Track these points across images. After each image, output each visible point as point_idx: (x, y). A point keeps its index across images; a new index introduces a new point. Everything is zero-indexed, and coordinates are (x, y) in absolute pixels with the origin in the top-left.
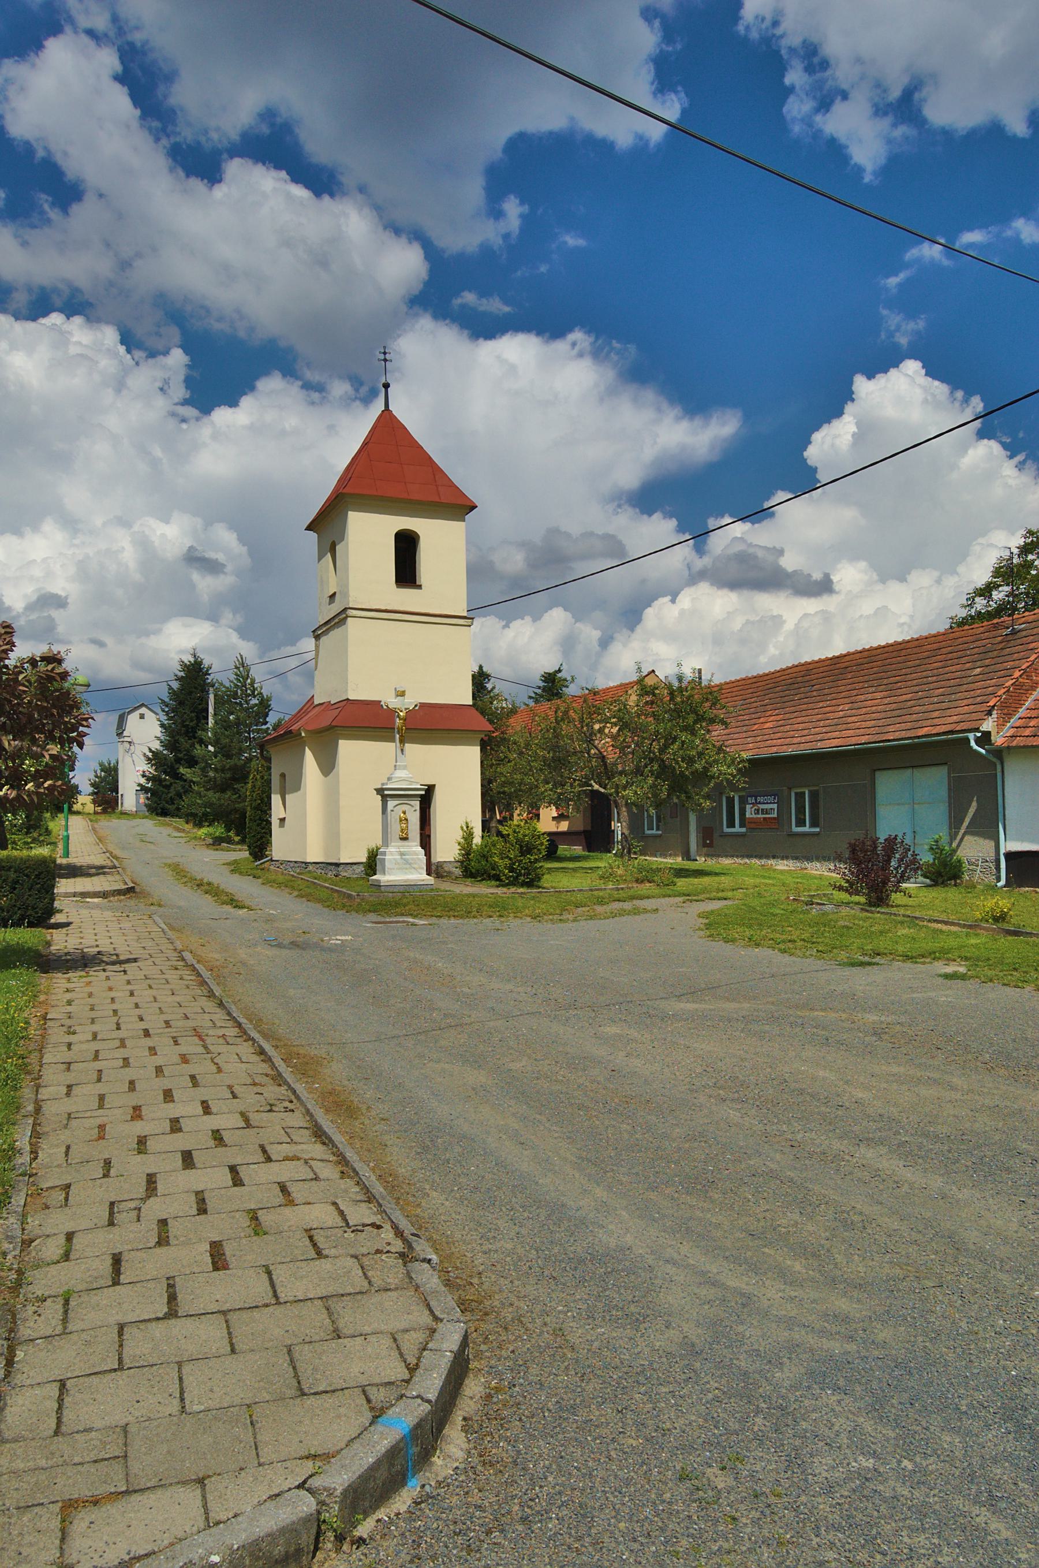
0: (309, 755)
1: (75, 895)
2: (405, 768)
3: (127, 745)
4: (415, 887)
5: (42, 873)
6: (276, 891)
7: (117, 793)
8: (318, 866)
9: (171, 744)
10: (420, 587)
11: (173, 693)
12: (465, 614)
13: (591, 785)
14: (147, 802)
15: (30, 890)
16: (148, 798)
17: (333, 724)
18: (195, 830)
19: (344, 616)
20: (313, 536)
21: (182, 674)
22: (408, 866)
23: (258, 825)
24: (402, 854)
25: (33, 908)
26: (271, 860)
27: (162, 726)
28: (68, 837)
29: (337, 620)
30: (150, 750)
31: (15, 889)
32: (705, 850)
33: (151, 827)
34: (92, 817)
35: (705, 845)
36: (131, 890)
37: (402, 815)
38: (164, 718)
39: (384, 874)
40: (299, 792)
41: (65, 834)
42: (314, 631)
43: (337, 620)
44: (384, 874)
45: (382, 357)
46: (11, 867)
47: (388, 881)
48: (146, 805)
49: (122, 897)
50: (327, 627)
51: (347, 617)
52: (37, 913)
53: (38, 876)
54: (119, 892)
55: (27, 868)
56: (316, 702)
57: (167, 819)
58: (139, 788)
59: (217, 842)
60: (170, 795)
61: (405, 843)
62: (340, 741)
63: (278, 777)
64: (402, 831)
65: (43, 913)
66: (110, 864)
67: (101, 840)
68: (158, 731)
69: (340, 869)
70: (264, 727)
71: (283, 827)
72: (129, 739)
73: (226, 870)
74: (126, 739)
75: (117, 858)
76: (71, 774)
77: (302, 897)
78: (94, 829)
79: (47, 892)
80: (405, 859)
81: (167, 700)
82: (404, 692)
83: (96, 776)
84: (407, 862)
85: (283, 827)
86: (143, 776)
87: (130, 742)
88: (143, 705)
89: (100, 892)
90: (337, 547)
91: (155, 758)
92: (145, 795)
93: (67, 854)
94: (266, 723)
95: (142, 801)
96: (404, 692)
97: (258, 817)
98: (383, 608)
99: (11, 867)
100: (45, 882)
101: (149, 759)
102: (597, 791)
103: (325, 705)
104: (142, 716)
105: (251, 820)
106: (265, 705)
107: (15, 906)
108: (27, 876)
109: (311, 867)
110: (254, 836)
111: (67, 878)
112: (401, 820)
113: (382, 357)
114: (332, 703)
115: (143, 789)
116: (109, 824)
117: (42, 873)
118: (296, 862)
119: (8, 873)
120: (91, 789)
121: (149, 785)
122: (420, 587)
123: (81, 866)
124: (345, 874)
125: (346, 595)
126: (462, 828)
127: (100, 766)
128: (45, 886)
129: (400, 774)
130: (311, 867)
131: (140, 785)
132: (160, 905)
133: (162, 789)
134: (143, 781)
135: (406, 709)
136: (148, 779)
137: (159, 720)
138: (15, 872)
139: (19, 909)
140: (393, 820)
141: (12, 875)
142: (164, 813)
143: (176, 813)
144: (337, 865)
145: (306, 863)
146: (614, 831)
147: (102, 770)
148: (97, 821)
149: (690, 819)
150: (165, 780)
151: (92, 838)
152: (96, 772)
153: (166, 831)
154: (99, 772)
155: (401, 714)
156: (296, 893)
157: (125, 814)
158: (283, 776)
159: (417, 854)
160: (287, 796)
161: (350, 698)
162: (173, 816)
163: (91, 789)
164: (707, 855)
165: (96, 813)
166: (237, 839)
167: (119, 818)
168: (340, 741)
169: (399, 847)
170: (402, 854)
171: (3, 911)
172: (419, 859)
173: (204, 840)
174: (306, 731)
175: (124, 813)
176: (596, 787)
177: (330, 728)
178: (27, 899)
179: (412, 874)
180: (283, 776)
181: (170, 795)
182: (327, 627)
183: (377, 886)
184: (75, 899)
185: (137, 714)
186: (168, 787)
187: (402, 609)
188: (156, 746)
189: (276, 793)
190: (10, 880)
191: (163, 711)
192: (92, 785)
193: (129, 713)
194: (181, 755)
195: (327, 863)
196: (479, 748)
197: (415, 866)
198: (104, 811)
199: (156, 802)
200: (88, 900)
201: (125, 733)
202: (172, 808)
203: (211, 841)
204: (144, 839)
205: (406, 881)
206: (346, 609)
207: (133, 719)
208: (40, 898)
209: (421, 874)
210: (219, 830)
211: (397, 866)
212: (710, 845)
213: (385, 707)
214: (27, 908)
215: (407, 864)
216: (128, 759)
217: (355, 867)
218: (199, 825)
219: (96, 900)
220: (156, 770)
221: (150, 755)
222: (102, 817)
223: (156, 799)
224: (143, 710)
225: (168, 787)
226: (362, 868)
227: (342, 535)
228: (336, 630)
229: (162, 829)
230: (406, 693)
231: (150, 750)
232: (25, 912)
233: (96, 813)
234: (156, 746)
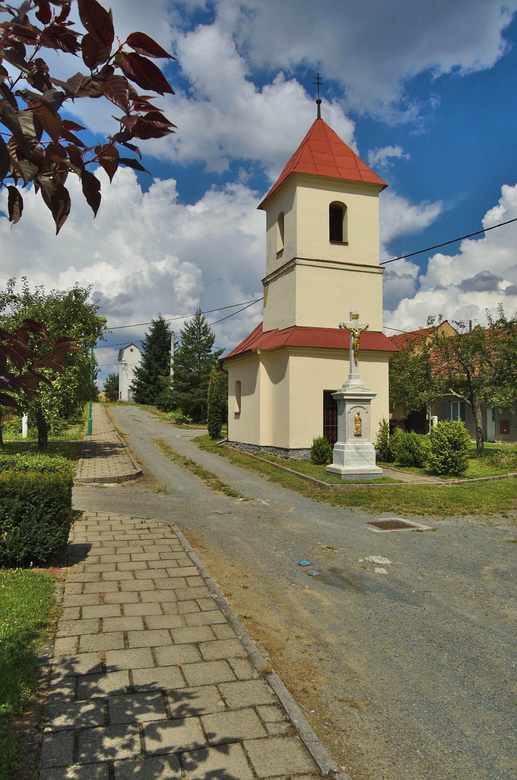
0: (262, 368)
1: (94, 480)
2: (358, 377)
3: (124, 365)
4: (368, 476)
5: (54, 500)
6: (247, 471)
7: (118, 391)
8: (268, 449)
9: (148, 364)
10: (346, 244)
11: (149, 338)
12: (378, 265)
13: (450, 392)
14: (134, 396)
15: (38, 521)
16: (134, 394)
17: (286, 344)
18: (163, 413)
19: (293, 264)
20: (263, 213)
21: (153, 327)
22: (362, 458)
23: (216, 416)
24: (357, 448)
25: (42, 544)
26: (227, 441)
27: (143, 355)
28: (91, 421)
29: (285, 269)
30: (136, 368)
31: (20, 520)
32: (502, 436)
33: (137, 410)
34: (106, 404)
35: (502, 432)
36: (140, 474)
37: (357, 416)
38: (143, 351)
39: (343, 465)
40: (253, 395)
41: (90, 419)
42: (263, 280)
43: (285, 269)
44: (343, 465)
45: (316, 81)
46: (15, 494)
47: (347, 471)
48: (133, 398)
49: (133, 481)
50: (276, 275)
51: (296, 264)
52: (46, 549)
53: (48, 505)
54: (130, 477)
55: (35, 494)
56: (264, 330)
57: (146, 406)
58: (130, 389)
59: (179, 422)
60: (146, 393)
61: (358, 439)
62: (290, 357)
63: (234, 384)
64: (357, 429)
65: (54, 550)
66: (119, 442)
67: (111, 420)
68: (140, 358)
69: (290, 453)
70: (209, 354)
71: (239, 418)
72: (125, 362)
73: (195, 446)
74: (123, 362)
75: (121, 435)
76: (95, 381)
77: (276, 481)
78: (106, 412)
79: (60, 523)
80: (359, 453)
81: (145, 342)
82: (358, 315)
83: (107, 382)
84: (361, 455)
85: (239, 418)
86: (133, 382)
87: (125, 364)
88: (132, 344)
89: (115, 478)
90: (285, 216)
91: (139, 373)
92: (133, 393)
93: (90, 433)
94: (210, 351)
95: (131, 395)
96: (358, 315)
97: (215, 411)
98: (321, 259)
99: (15, 494)
100: (57, 512)
101: (135, 373)
102: (455, 396)
103: (272, 333)
104: (132, 350)
105: (210, 412)
106: (211, 341)
107: (20, 541)
108: (35, 504)
109: (262, 450)
110: (212, 423)
111: (89, 458)
112: (356, 420)
113: (316, 81)
114: (280, 330)
115: (133, 389)
116: (114, 408)
117: (54, 500)
118: (250, 445)
119: (12, 500)
120: (105, 389)
121: (136, 387)
122: (346, 244)
123: (100, 444)
124: (293, 457)
125: (294, 248)
126: (380, 423)
127: (110, 376)
128: (58, 516)
129: (354, 382)
130: (262, 450)
131: (130, 387)
132: (166, 493)
133: (142, 389)
134: (132, 384)
135: (359, 329)
136: (135, 384)
137: (141, 352)
138: (20, 499)
139: (25, 544)
140: (349, 420)
141: (17, 504)
142: (143, 402)
143: (151, 402)
144: (287, 450)
145: (259, 447)
146: (428, 421)
147: (110, 379)
148: (107, 407)
149: (488, 415)
150: (144, 384)
151: (105, 419)
152: (107, 379)
153: (147, 413)
154: (109, 380)
155: (356, 333)
156: (268, 477)
157: (123, 402)
158: (239, 383)
159: (368, 449)
160: (242, 397)
161: (297, 325)
162: (148, 404)
163: (105, 389)
164: (504, 440)
165: (107, 402)
166: (190, 420)
167: (119, 405)
168: (290, 357)
169: (354, 442)
170: (357, 448)
171: (5, 548)
172: (370, 452)
173: (170, 420)
174: (261, 350)
175: (122, 402)
176: (454, 394)
177: (284, 347)
178: (36, 532)
179: (365, 464)
180: (239, 383)
181: (146, 393)
182: (276, 275)
183: (338, 474)
184: (95, 484)
185: (129, 349)
186: (146, 388)
187: (334, 260)
188: (139, 366)
189: (232, 395)
190: (15, 508)
191: (143, 347)
192: (105, 387)
193: (125, 348)
194: (153, 371)
195: (277, 448)
196: (388, 364)
197: (367, 458)
198: (111, 400)
199: (139, 396)
200: (106, 485)
201: (123, 359)
202: (147, 399)
203: (174, 421)
204: (135, 419)
205: (361, 470)
206: (295, 259)
207: (127, 351)
208: (51, 531)
209: (371, 465)
210: (178, 414)
211: (353, 458)
212: (508, 433)
213: (343, 328)
214: (34, 544)
215: (361, 457)
216: (124, 373)
217: (300, 452)
218: (165, 411)
219: (112, 485)
220: (139, 379)
221: (136, 370)
222: (110, 404)
223: (138, 394)
224: (132, 347)
225: (146, 388)
226: (308, 453)
227: (290, 204)
228: (284, 277)
229: (144, 412)
230: (360, 316)
231: (136, 368)
232: (33, 549)
233: (107, 402)
234: (139, 366)
